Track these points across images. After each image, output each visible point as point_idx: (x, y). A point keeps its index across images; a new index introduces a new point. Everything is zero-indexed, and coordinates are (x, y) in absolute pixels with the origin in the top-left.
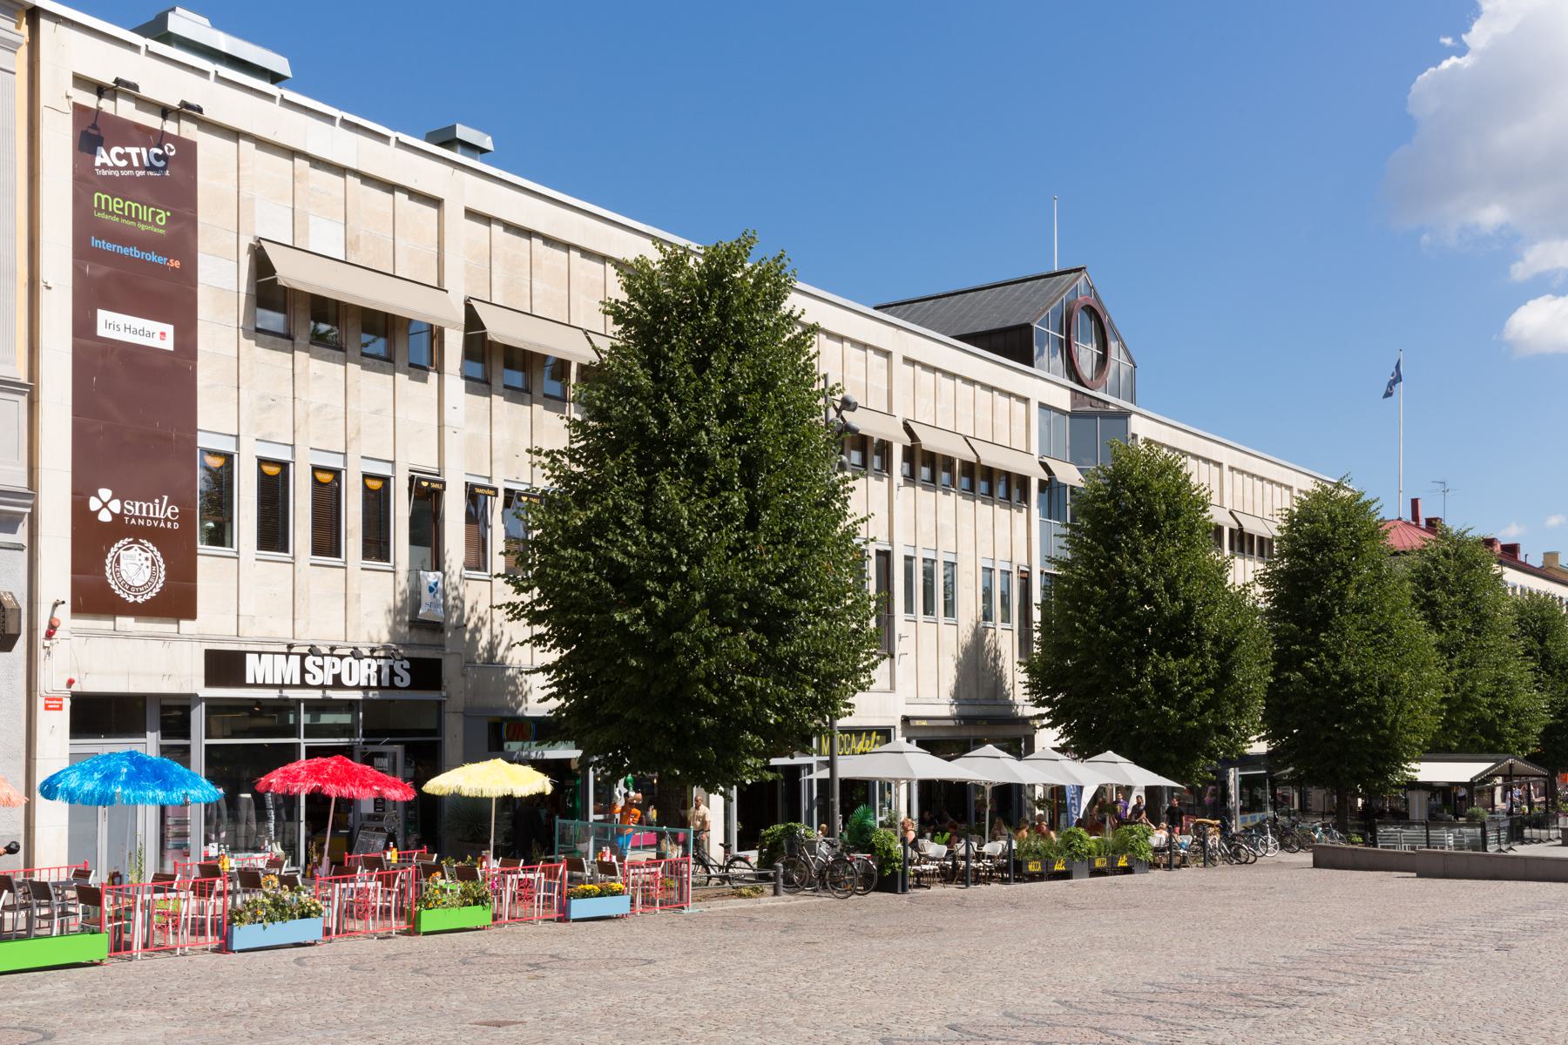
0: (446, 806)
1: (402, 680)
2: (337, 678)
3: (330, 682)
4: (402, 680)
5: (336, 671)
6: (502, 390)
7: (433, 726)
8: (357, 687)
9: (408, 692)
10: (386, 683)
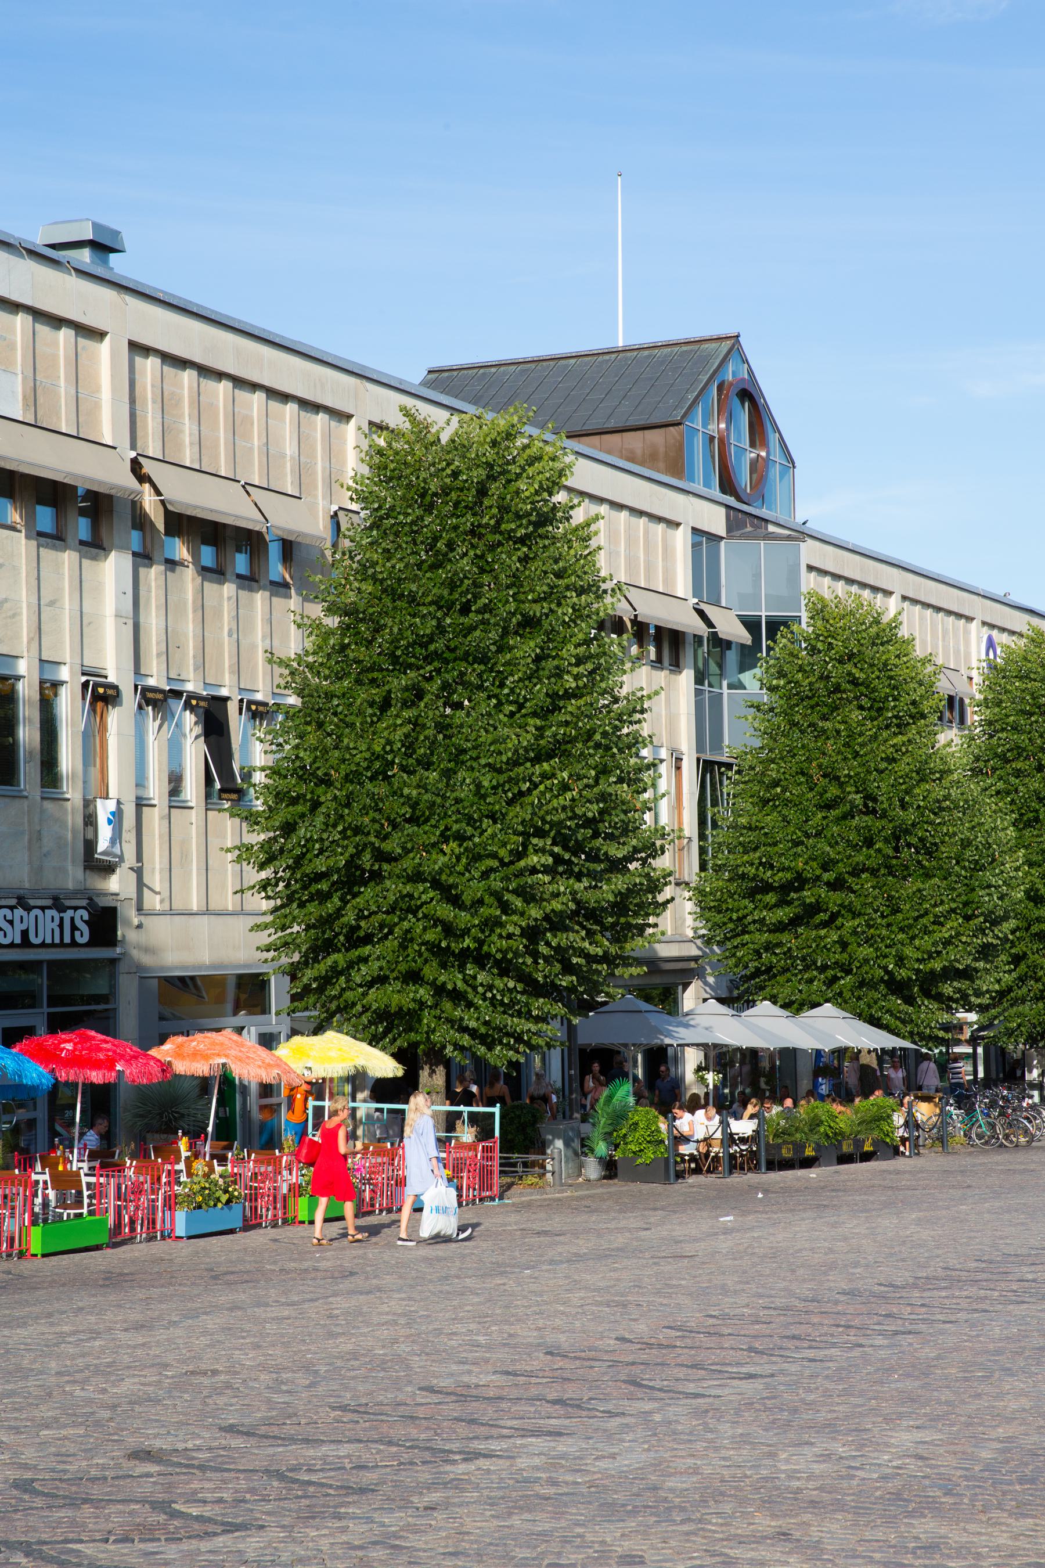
0: (122, 1101)
1: (82, 936)
2: (25, 933)
3: (18, 940)
4: (82, 936)
5: (24, 927)
6: (234, 577)
7: (104, 991)
8: (43, 945)
9: (87, 949)
10: (67, 940)
